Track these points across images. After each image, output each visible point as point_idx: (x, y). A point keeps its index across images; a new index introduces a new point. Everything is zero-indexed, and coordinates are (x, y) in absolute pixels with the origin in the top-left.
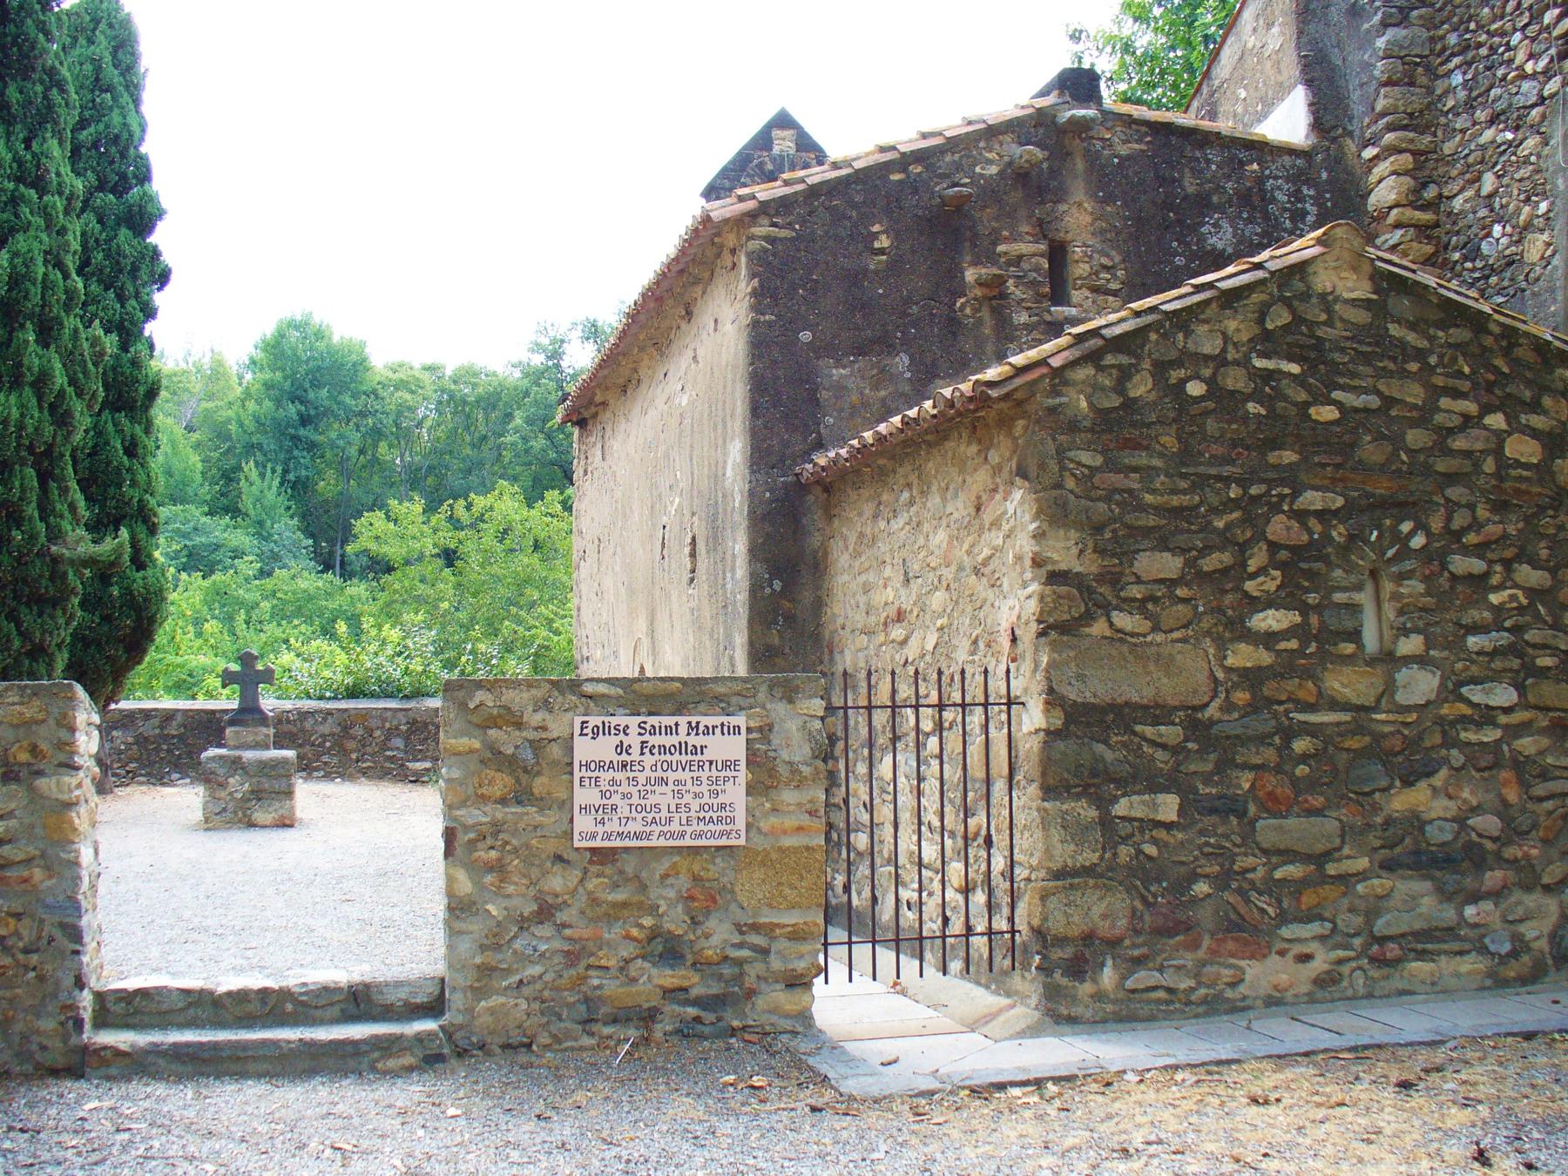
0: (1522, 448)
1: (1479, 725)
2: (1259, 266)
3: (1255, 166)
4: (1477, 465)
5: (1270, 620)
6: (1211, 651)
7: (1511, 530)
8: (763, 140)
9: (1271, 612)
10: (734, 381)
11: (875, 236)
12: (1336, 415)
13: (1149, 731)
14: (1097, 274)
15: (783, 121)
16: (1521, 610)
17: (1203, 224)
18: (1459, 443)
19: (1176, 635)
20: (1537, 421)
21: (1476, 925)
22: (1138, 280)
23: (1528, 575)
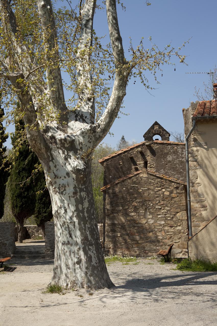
0: (167, 193)
1: (159, 226)
2: (126, 177)
4: (160, 195)
7: (165, 203)
8: (153, 127)
11: (120, 163)
14: (151, 165)
15: (156, 123)
16: (166, 212)
17: (167, 157)
18: (158, 193)
20: (169, 190)
21: (158, 249)
22: (157, 166)
23: (167, 208)
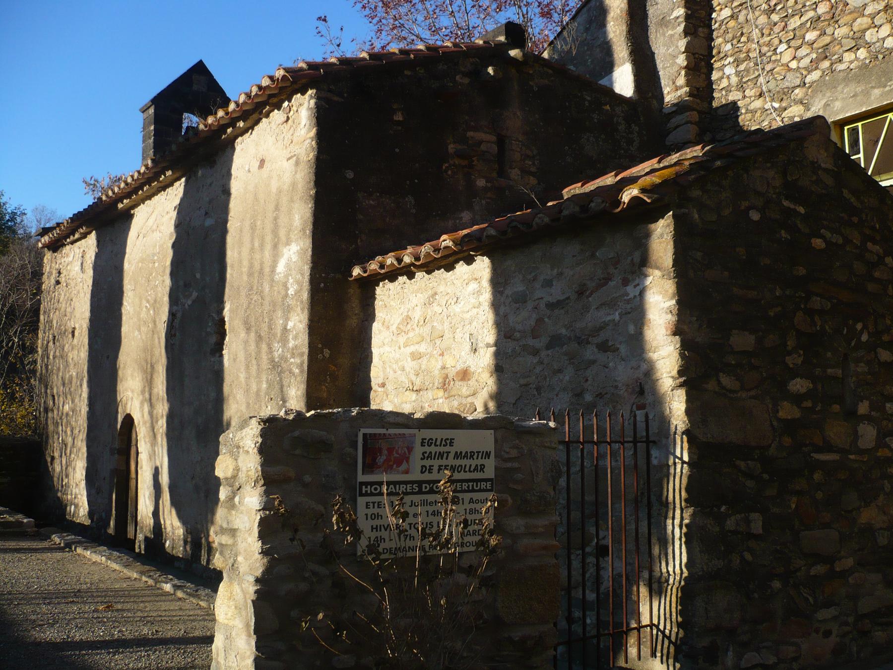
3: (608, 107)
5: (799, 385)
6: (770, 406)
9: (798, 380)
10: (292, 201)
12: (823, 245)
13: (742, 464)
15: (200, 68)
19: (753, 393)
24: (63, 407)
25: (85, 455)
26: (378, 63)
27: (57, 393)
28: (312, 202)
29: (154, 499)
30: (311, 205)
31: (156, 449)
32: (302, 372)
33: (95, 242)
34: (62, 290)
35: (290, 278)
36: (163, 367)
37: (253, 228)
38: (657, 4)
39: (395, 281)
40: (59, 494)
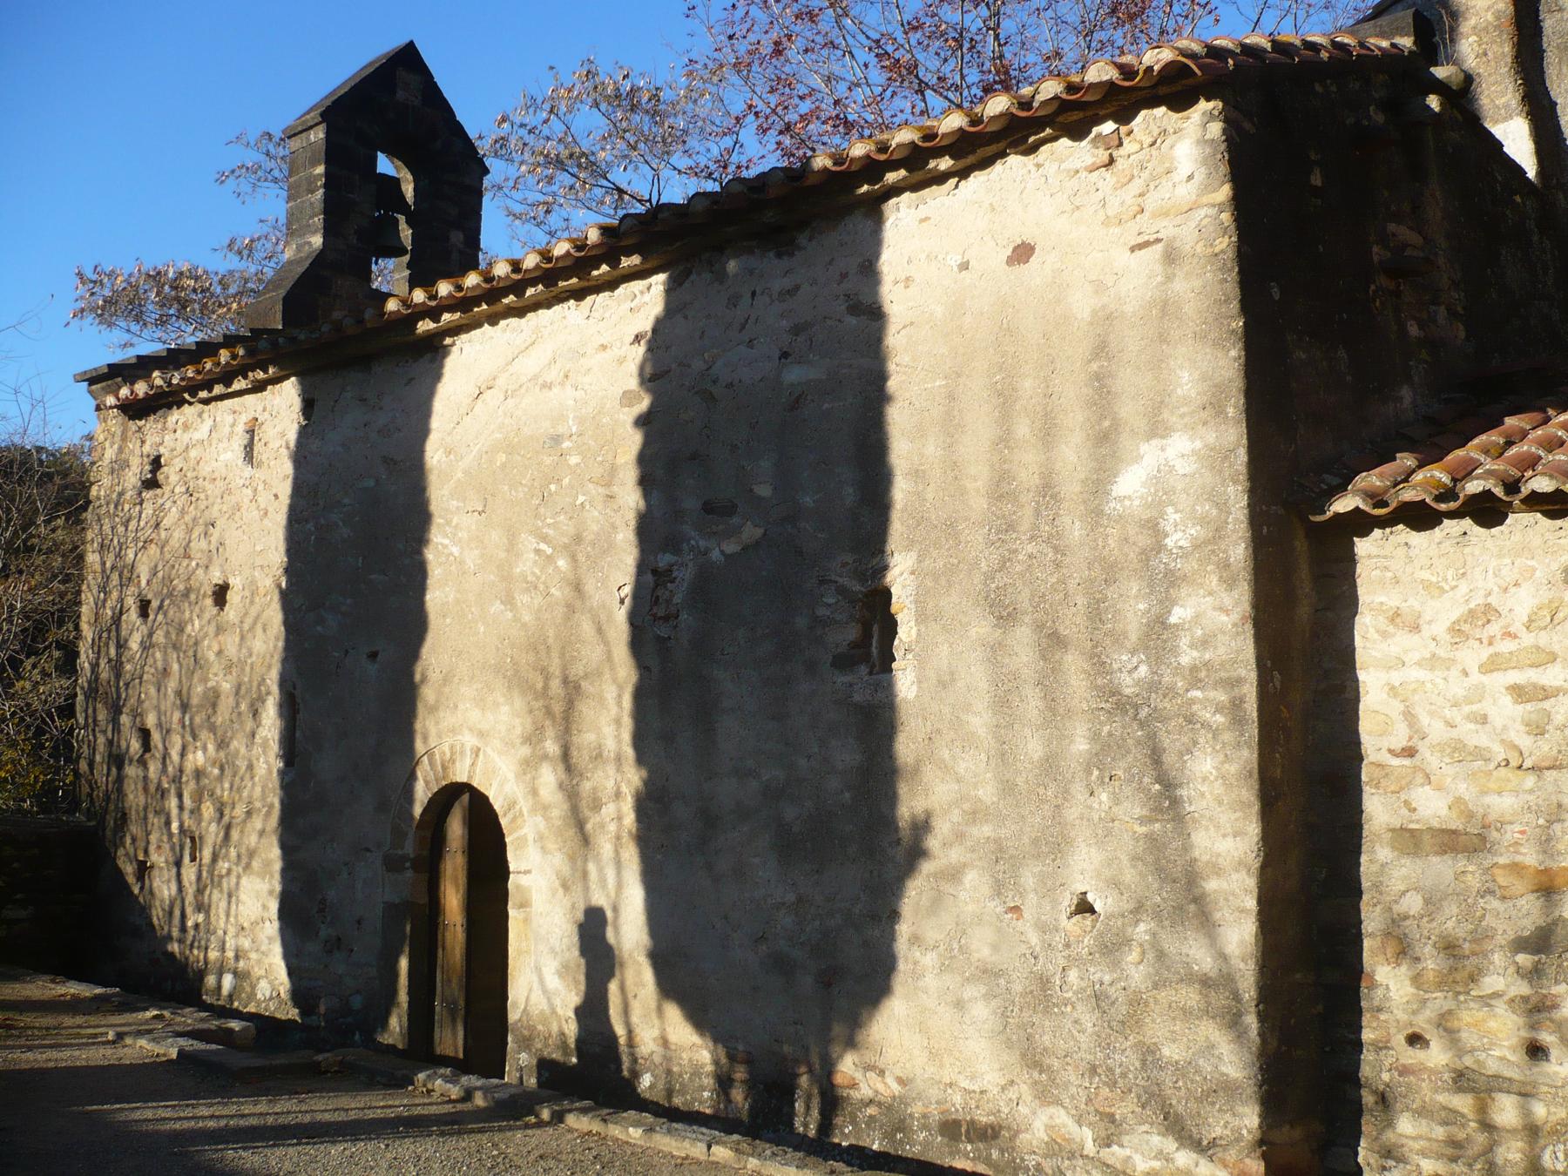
15: (407, 59)
24: (183, 754)
25: (277, 866)
26: (1283, 59)
27: (160, 725)
28: (1240, 345)
29: (582, 978)
30: (1235, 352)
31: (591, 867)
32: (1238, 721)
33: (297, 403)
34: (170, 504)
35: (1170, 510)
36: (621, 688)
37: (1005, 399)
38: (1561, 10)
39: (1432, 527)
40: (174, 947)
